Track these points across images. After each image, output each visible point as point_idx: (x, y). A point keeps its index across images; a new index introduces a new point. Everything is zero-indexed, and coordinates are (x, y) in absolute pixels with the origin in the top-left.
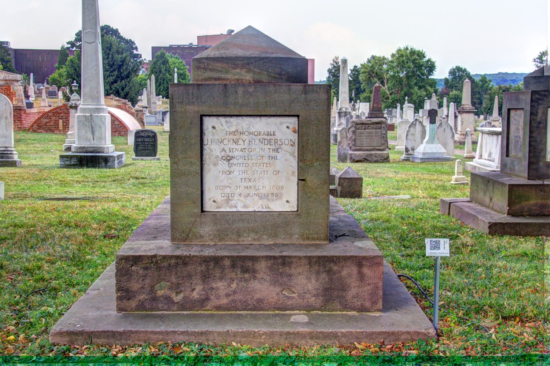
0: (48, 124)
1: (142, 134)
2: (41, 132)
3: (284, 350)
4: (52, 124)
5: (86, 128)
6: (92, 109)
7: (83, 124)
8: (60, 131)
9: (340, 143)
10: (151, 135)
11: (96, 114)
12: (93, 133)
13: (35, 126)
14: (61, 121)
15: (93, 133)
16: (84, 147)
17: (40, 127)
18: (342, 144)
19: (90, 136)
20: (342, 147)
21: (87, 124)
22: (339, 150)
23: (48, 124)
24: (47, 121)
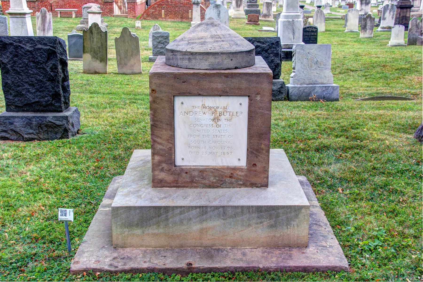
0: (154, 13)
1: (307, 30)
2: (149, 19)
3: (30, 204)
4: (157, 13)
5: (289, 30)
6: (293, 15)
7: (287, 27)
8: (163, 18)
9: (411, 29)
10: (314, 30)
11: (296, 20)
12: (294, 34)
13: (145, 15)
14: (163, 11)
15: (294, 34)
16: (287, 45)
17: (148, 16)
18: (412, 31)
19: (291, 36)
20: (412, 33)
21: (290, 27)
22: (409, 35)
23: (154, 13)
24: (154, 11)
